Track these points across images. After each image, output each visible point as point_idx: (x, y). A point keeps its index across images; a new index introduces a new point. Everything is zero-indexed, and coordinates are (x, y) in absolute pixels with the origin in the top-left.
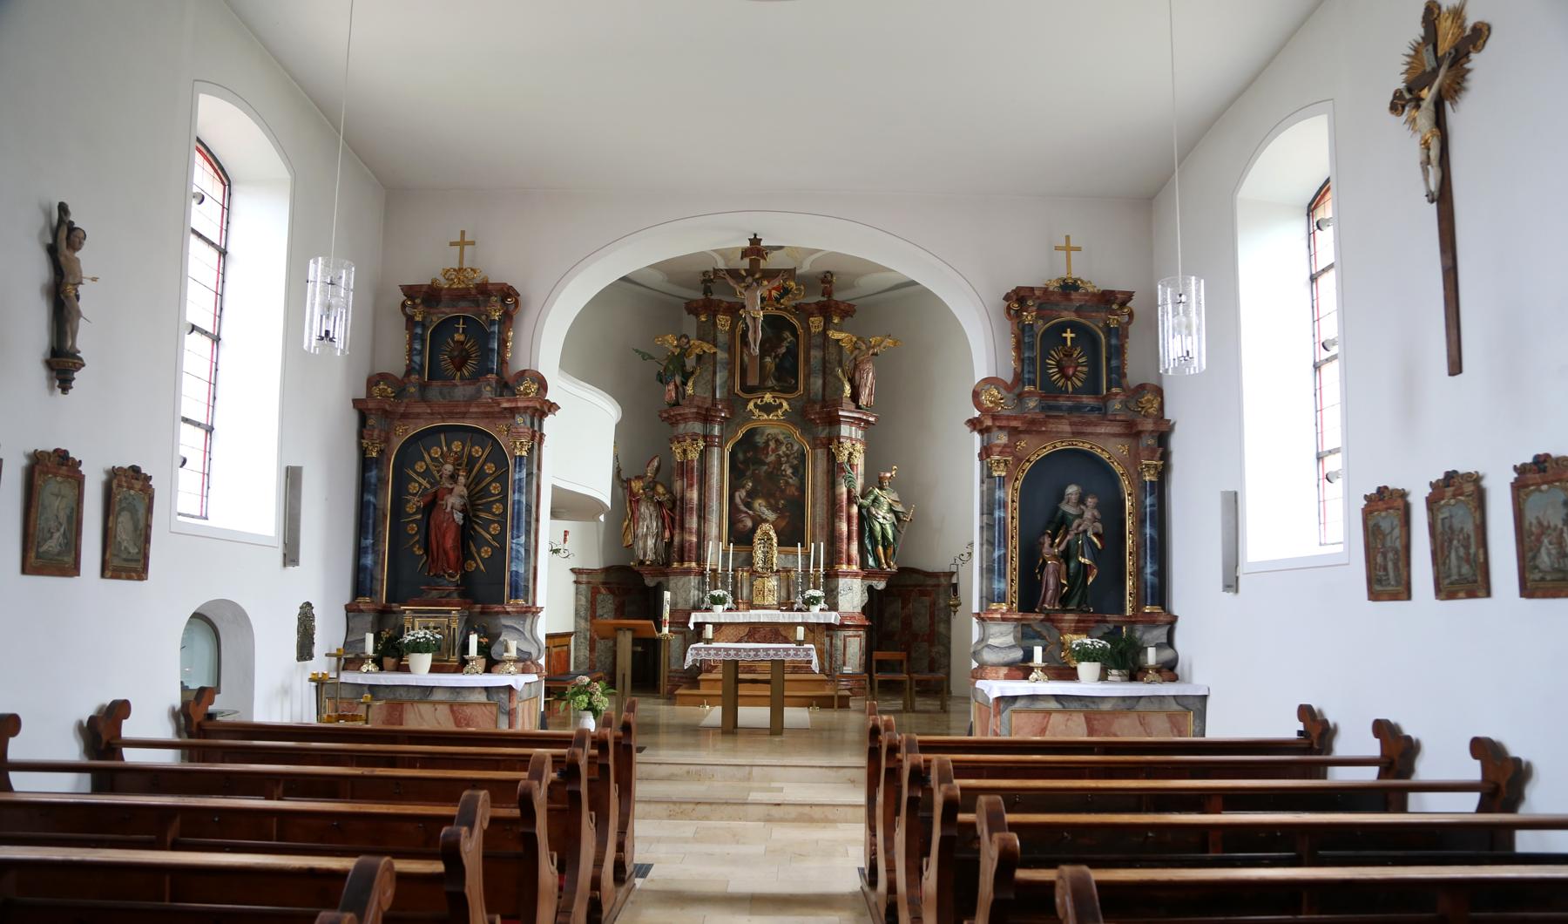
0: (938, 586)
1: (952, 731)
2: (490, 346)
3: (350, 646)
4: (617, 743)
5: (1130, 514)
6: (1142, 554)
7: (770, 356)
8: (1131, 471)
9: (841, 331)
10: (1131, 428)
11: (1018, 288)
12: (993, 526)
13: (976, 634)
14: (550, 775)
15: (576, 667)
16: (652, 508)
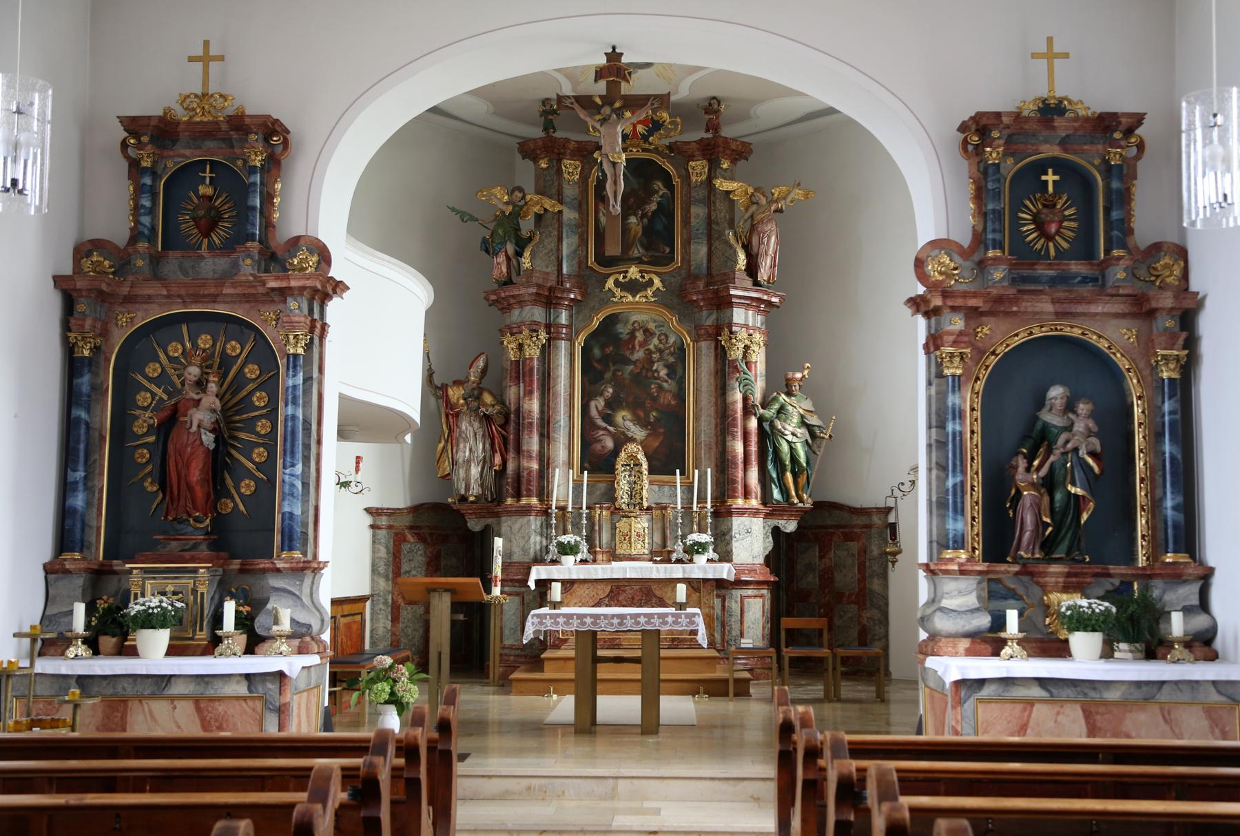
0: (869, 526)
1: (893, 729)
2: (250, 203)
3: (50, 621)
4: (431, 748)
5: (1140, 424)
6: (1159, 480)
7: (635, 215)
8: (1142, 365)
9: (732, 179)
11: (978, 114)
13: (924, 595)
14: (338, 796)
15: (373, 643)
16: (476, 424)
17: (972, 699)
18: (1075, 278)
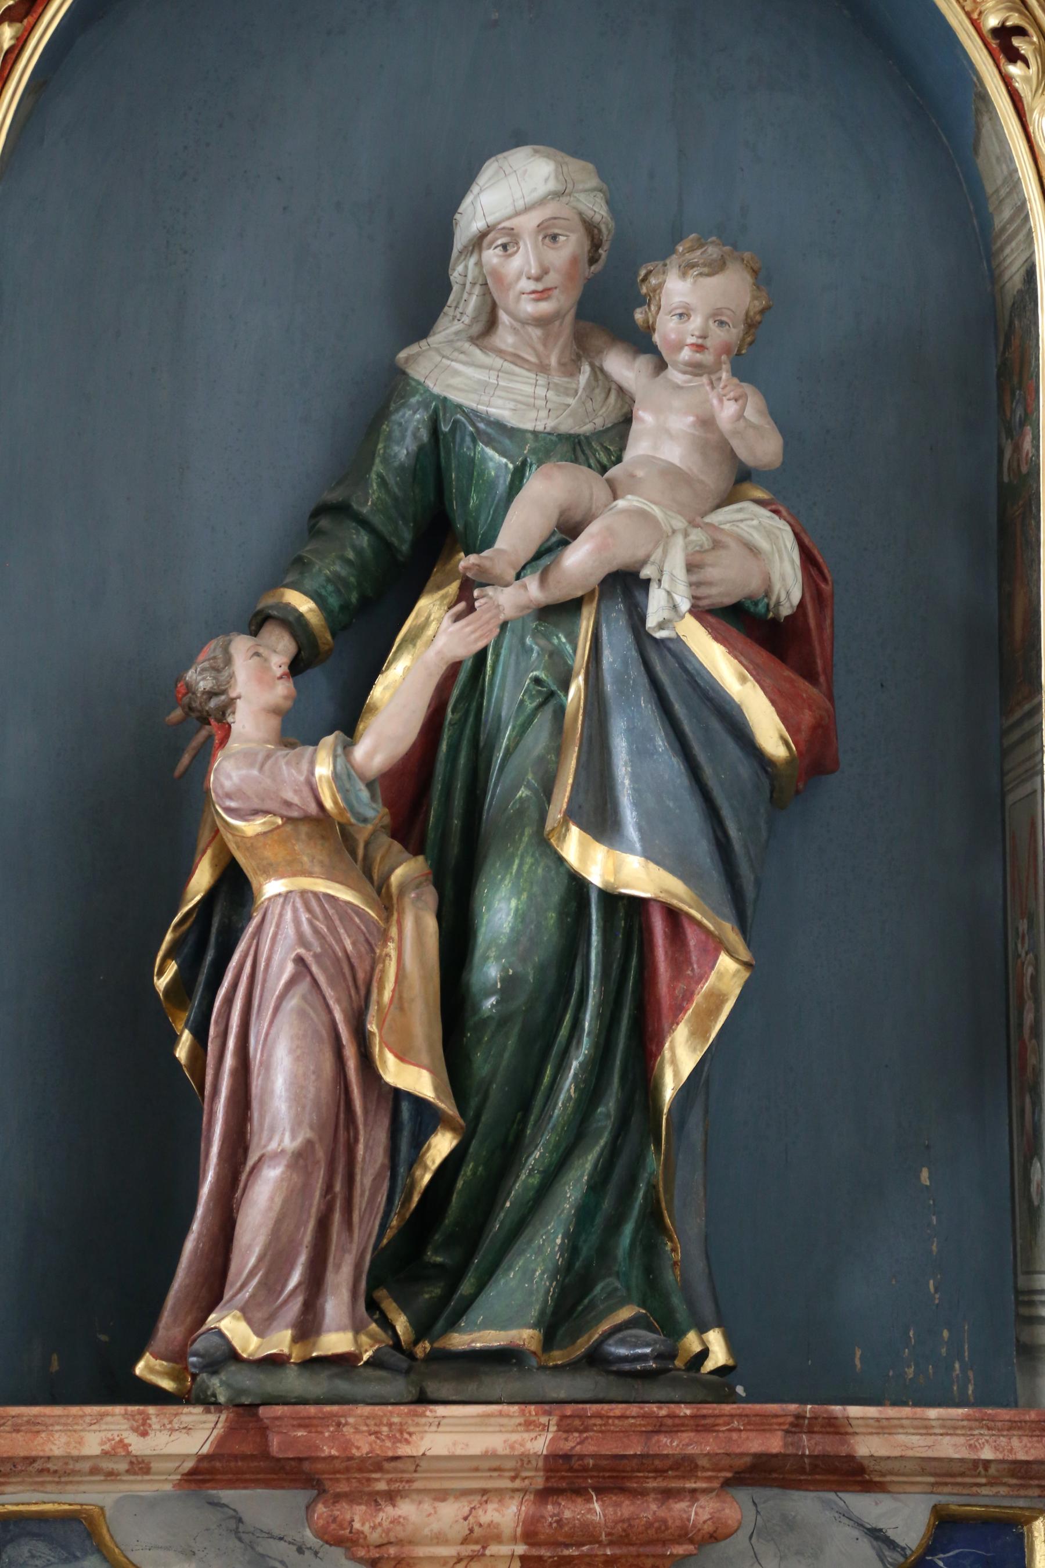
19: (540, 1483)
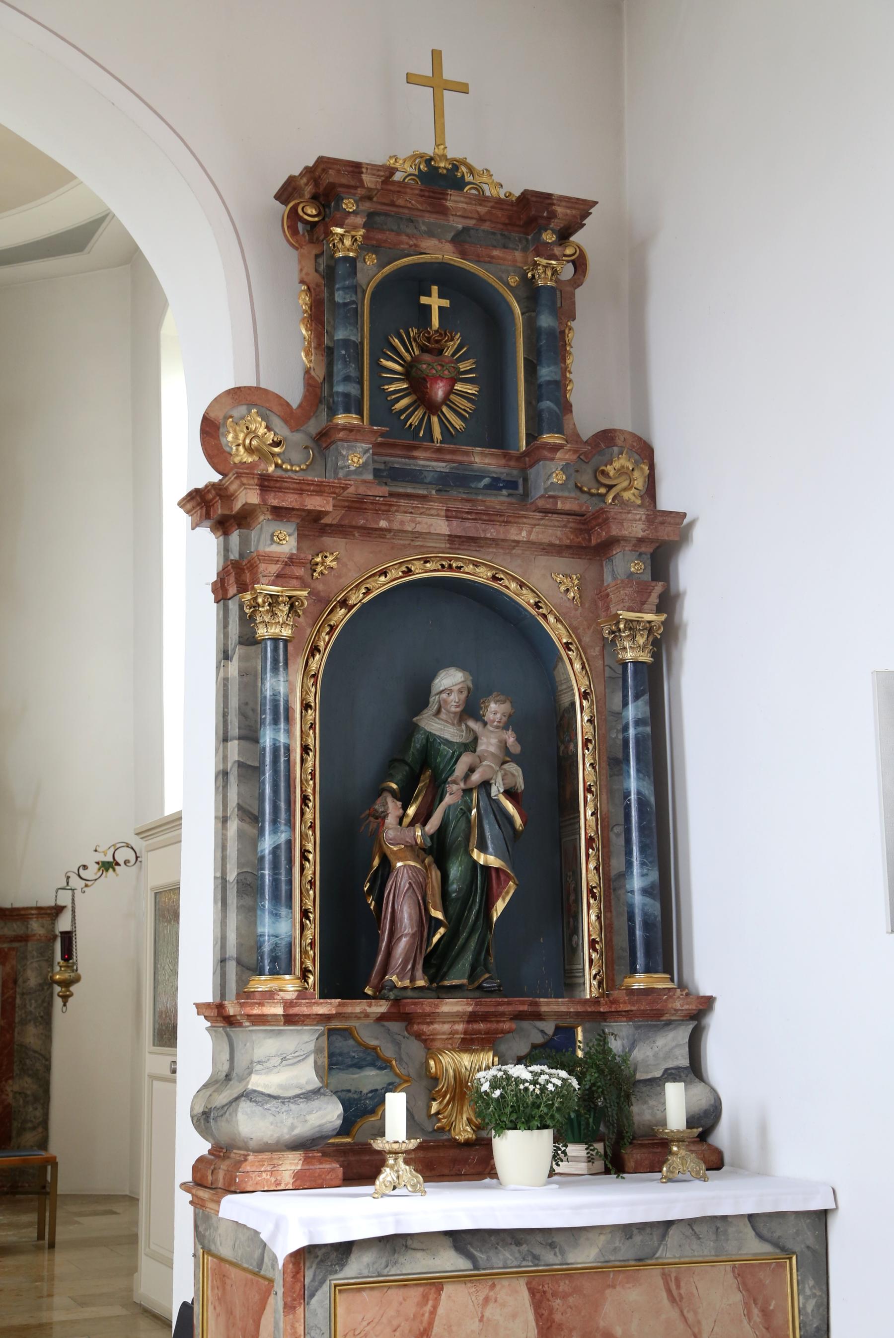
0: (24, 939)
5: (586, 742)
10: (589, 531)
11: (321, 161)
12: (258, 770)
17: (325, 1287)
18: (480, 478)
19: (466, 1019)
